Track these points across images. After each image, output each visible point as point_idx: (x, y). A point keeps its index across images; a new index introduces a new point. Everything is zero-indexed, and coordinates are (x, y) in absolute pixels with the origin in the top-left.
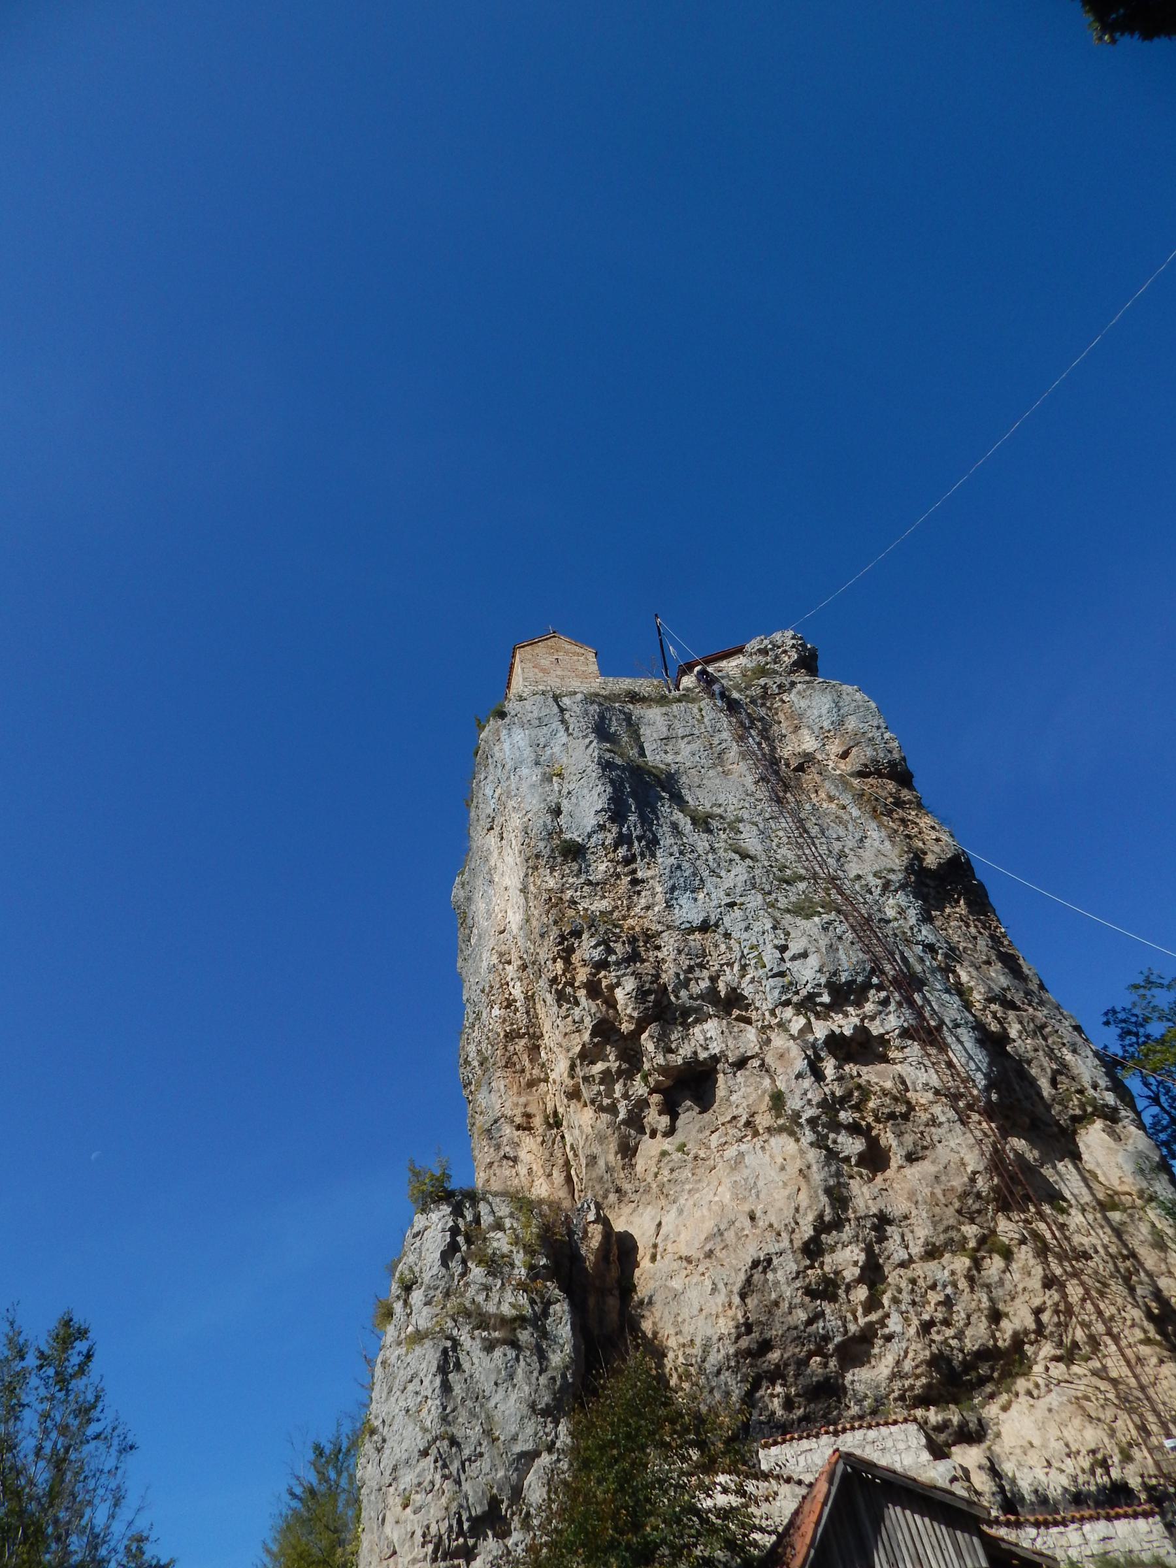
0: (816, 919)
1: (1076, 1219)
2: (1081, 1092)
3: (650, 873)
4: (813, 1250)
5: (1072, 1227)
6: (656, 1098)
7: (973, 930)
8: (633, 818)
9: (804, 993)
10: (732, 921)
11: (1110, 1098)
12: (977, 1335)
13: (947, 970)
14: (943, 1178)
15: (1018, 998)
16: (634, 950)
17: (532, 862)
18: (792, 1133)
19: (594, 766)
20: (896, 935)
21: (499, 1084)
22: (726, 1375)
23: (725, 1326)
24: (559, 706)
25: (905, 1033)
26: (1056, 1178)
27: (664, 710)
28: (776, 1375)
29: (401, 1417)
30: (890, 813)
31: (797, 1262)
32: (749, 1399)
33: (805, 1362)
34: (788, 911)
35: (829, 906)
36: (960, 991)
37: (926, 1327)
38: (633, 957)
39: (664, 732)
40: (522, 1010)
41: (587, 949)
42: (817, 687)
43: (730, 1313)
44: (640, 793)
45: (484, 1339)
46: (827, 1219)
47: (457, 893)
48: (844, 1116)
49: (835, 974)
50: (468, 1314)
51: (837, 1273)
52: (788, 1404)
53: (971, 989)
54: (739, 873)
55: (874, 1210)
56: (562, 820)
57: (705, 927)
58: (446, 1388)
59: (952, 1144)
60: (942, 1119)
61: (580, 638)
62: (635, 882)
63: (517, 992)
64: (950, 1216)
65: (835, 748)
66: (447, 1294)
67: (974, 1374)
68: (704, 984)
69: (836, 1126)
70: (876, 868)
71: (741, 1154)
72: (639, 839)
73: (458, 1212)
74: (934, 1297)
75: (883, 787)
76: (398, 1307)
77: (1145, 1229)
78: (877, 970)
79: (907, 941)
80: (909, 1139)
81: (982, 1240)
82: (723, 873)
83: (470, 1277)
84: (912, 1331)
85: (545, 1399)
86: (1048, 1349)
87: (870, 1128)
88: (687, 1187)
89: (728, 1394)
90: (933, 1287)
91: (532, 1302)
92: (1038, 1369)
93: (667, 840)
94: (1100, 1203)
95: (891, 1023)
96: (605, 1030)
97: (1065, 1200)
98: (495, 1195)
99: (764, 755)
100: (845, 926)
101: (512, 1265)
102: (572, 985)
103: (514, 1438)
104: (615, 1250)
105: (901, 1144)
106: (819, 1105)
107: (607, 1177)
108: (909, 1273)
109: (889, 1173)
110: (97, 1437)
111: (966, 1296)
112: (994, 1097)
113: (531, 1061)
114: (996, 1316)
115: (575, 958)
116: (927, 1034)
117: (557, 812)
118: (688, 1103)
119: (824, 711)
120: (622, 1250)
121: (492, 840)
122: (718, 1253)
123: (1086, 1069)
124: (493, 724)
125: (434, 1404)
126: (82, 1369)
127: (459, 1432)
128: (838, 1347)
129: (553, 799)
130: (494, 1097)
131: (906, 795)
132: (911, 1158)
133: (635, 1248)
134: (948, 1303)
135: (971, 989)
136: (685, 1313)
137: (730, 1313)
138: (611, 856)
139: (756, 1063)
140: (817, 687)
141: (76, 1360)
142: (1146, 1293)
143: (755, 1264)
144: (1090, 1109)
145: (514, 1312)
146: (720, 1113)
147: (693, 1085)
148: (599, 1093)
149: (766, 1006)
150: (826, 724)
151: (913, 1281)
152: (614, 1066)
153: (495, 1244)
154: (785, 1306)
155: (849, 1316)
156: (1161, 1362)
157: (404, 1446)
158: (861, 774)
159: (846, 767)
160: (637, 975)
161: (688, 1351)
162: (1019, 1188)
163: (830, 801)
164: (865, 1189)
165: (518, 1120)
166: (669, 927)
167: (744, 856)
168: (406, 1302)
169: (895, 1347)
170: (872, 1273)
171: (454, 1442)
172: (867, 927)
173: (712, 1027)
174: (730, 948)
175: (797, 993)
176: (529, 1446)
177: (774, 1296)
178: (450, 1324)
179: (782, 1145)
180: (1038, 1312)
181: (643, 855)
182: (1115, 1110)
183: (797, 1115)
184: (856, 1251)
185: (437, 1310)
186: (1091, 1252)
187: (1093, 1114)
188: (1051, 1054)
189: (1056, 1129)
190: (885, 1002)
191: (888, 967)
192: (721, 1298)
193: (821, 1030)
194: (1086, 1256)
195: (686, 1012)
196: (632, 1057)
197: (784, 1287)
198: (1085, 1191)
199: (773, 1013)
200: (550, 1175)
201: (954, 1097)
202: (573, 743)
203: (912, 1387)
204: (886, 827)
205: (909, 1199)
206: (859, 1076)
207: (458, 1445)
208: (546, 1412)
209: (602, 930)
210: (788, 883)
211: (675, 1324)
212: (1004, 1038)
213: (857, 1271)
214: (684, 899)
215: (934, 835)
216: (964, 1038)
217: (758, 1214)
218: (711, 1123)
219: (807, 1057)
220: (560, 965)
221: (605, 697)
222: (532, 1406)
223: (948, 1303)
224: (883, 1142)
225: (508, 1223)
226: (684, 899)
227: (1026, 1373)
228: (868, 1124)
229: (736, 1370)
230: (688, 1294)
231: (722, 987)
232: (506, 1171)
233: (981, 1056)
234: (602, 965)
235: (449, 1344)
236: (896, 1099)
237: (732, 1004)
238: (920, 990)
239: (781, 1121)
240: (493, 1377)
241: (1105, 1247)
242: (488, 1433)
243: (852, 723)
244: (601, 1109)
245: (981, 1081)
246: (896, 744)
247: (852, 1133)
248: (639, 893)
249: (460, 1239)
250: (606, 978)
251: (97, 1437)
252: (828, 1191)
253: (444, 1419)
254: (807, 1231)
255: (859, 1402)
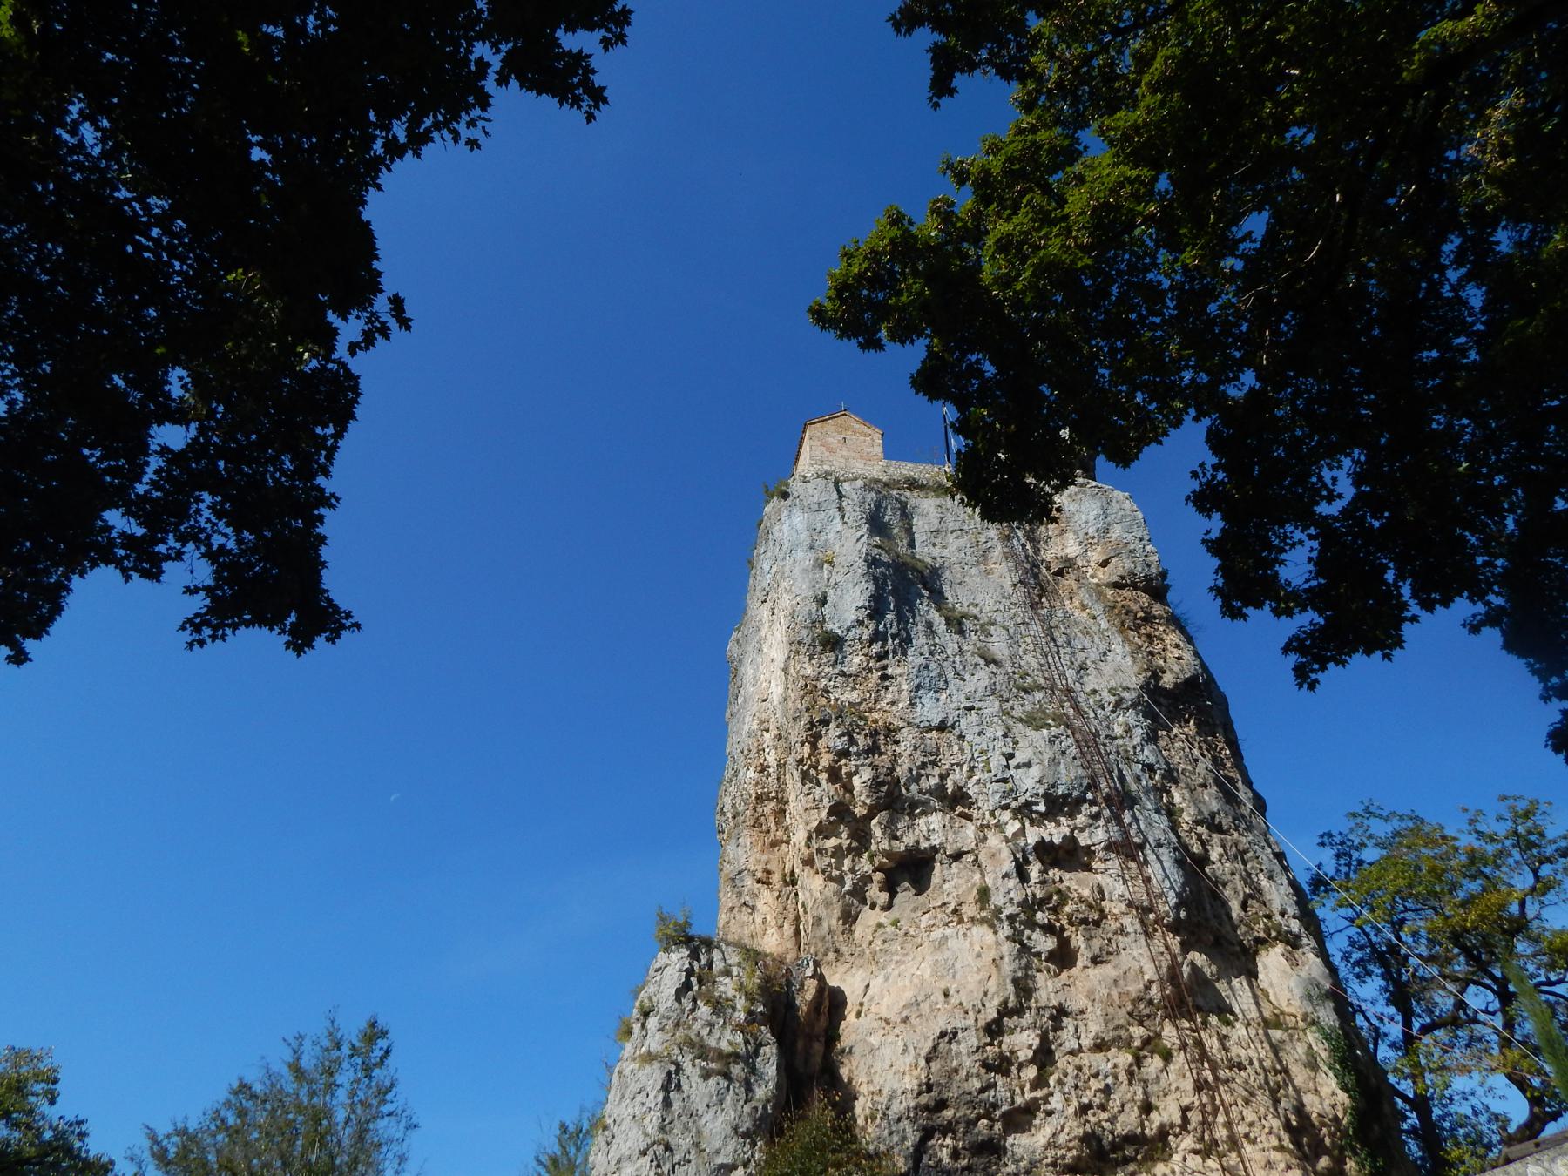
0: (1045, 731)
1: (1239, 1031)
2: (1269, 917)
3: (899, 671)
4: (994, 1030)
5: (1234, 1039)
6: (878, 876)
7: (1196, 752)
8: (890, 616)
9: (1022, 800)
10: (968, 724)
11: (1295, 926)
12: (1128, 1122)
13: (1162, 790)
14: (1121, 982)
15: (1226, 822)
16: (874, 742)
17: (795, 646)
18: (992, 926)
19: (861, 563)
20: (1118, 753)
21: (746, 841)
22: (905, 1123)
23: (910, 1083)
24: (839, 492)
25: (1110, 847)
26: (1229, 992)
27: (938, 501)
28: (948, 1129)
29: (628, 1122)
30: (1137, 629)
31: (979, 1039)
32: (920, 1149)
33: (975, 1123)
34: (1021, 720)
35: (1060, 719)
36: (1171, 812)
37: (1084, 1109)
38: (873, 750)
39: (935, 525)
40: (774, 775)
41: (832, 738)
42: (1089, 491)
43: (915, 1073)
44: (902, 587)
45: (702, 1068)
46: (1010, 1005)
47: (732, 649)
48: (1041, 917)
49: (1053, 786)
50: (692, 1045)
51: (1012, 1052)
52: (955, 1155)
53: (1182, 810)
54: (980, 679)
55: (1054, 1003)
56: (827, 610)
57: (942, 727)
58: (667, 1103)
59: (1135, 953)
60: (1130, 929)
61: (869, 419)
62: (884, 677)
63: (771, 759)
64: (1121, 1017)
65: (1096, 556)
66: (677, 1025)
67: (1120, 1154)
68: (934, 781)
69: (1032, 924)
70: (1113, 684)
71: (945, 938)
72: (894, 637)
73: (694, 955)
74: (1095, 1084)
75: (1136, 601)
76: (637, 1027)
77: (1301, 1049)
78: (1093, 786)
79: (1128, 760)
80: (1097, 944)
81: (1147, 1042)
82: (967, 677)
83: (698, 1013)
84: (1071, 1110)
85: (747, 1124)
86: (1188, 1142)
87: (1063, 929)
88: (895, 958)
89: (904, 1138)
90: (1096, 1075)
91: (747, 1042)
92: (1177, 1158)
93: (919, 640)
94: (1265, 1021)
95: (1097, 836)
96: (840, 811)
97: (1232, 1013)
98: (728, 945)
99: (1027, 557)
100: (1071, 741)
101: (734, 1009)
102: (816, 768)
103: (718, 1152)
104: (827, 1003)
105: (1089, 947)
106: (1019, 905)
107: (828, 937)
108: (1076, 1061)
109: (1074, 971)
110: (390, 1114)
111: (1124, 1087)
112: (1183, 914)
113: (777, 823)
114: (1147, 1108)
115: (821, 744)
116: (1128, 849)
117: (822, 601)
118: (907, 884)
119: (1091, 517)
120: (832, 1003)
121: (764, 612)
122: (912, 1020)
123: (1278, 895)
124: (775, 502)
125: (655, 1116)
126: (381, 1063)
127: (673, 1142)
128: (1004, 1115)
129: (821, 586)
130: (740, 851)
131: (1158, 610)
132: (1096, 961)
133: (844, 1003)
134: (1107, 1091)
135: (1182, 810)
136: (878, 1067)
137: (915, 1073)
138: (866, 650)
139: (970, 858)
140: (1089, 491)
141: (378, 1053)
142: (1289, 1106)
143: (943, 1035)
144: (1274, 934)
145: (730, 1049)
146: (933, 897)
147: (912, 870)
148: (830, 865)
149: (987, 807)
150: (1091, 531)
151: (1079, 1069)
152: (846, 843)
153: (722, 989)
154: (963, 1074)
155: (1018, 1090)
156: (1289, 1167)
157: (629, 1144)
158: (1117, 586)
159: (1105, 576)
160: (874, 767)
161: (876, 1098)
162: (1191, 999)
163: (1081, 609)
164: (1049, 983)
165: (759, 875)
166: (909, 724)
167: (990, 661)
168: (643, 1026)
169: (1054, 1122)
170: (1044, 1057)
171: (668, 1148)
172: (1089, 744)
173: (936, 820)
174: (962, 750)
175: (1016, 799)
176: (729, 1160)
177: (955, 1064)
178: (677, 1051)
179: (982, 933)
180: (1185, 1110)
181: (895, 653)
182: (1298, 937)
183: (999, 910)
184: (1033, 1036)
185: (668, 1037)
186: (1246, 1063)
187: (1276, 938)
188: (1247, 879)
189: (1238, 948)
190: (1096, 817)
191: (1103, 785)
192: (910, 1059)
193: (1032, 836)
194: (1241, 1067)
195: (914, 804)
196: (861, 837)
197: (964, 1058)
198: (1253, 1007)
199: (992, 814)
200: (781, 926)
201: (1143, 911)
202: (848, 533)
203: (1063, 1157)
204: (1131, 642)
205: (1088, 997)
206: (1061, 881)
207: (671, 1151)
208: (746, 1135)
209: (848, 721)
210: (1026, 692)
211: (868, 1074)
212: (1203, 860)
213: (1030, 1053)
214: (928, 698)
215: (1177, 653)
216: (1164, 858)
217: (952, 992)
218: (923, 904)
219: (1016, 859)
220: (807, 748)
221: (886, 485)
222: (735, 1129)
223: (1107, 1091)
224: (1073, 943)
225: (735, 971)
226: (928, 698)
227: (1166, 1160)
228: (1062, 927)
229: (914, 1120)
230: (883, 1050)
231: (949, 785)
232: (744, 916)
233: (1176, 876)
234: (844, 754)
235: (673, 1068)
236: (1090, 906)
237: (956, 801)
238: (1131, 808)
239: (984, 914)
240: (706, 1101)
241: (1261, 1061)
242: (697, 1145)
243: (1116, 533)
244: (830, 878)
245: (1173, 900)
246: (1156, 558)
247: (1046, 933)
248: (887, 688)
249: (694, 980)
250: (847, 766)
251: (390, 1114)
252: (1015, 981)
253: (662, 1129)
254: (991, 1014)
255: (1016, 1162)
